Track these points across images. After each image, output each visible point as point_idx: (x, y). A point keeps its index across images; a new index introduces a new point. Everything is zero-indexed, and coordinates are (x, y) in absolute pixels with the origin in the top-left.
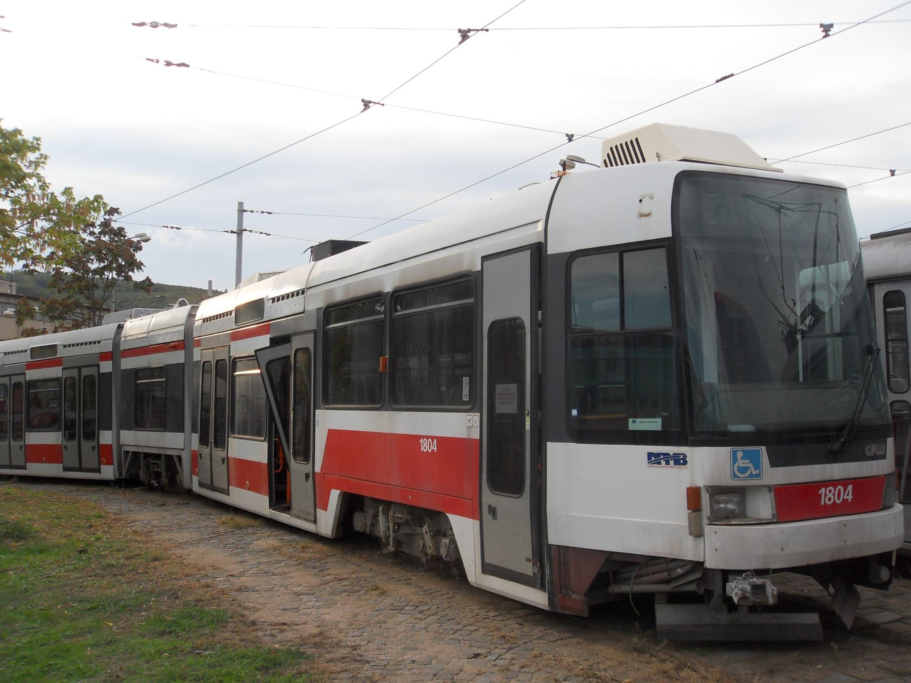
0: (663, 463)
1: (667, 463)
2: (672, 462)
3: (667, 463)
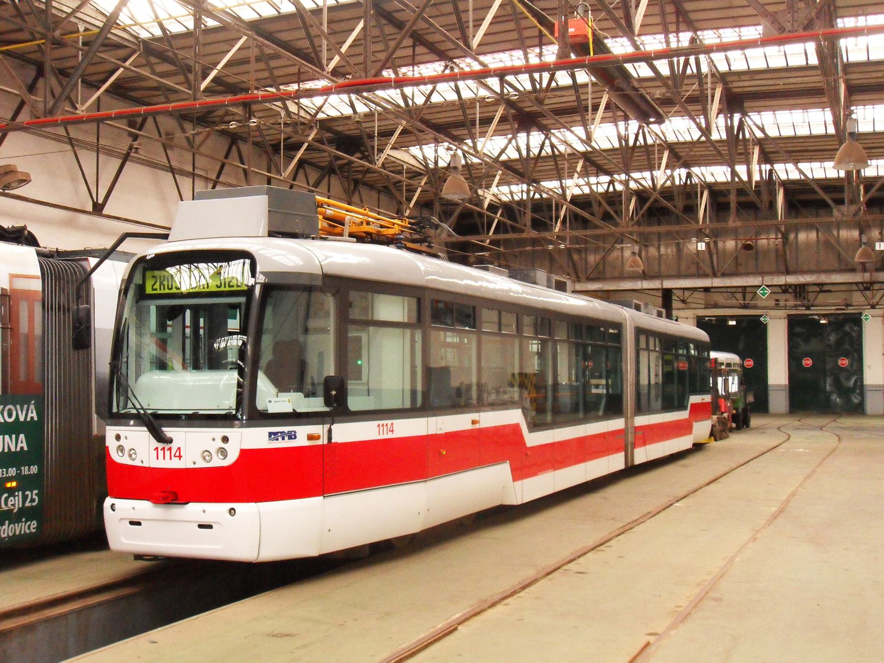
0: (280, 439)
1: (283, 439)
2: (286, 438)
3: (283, 439)
